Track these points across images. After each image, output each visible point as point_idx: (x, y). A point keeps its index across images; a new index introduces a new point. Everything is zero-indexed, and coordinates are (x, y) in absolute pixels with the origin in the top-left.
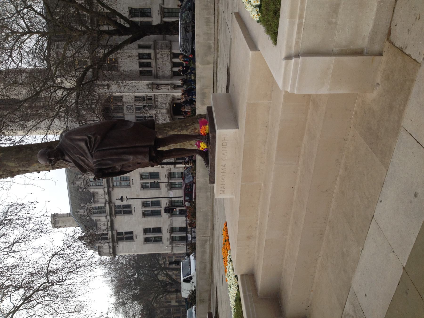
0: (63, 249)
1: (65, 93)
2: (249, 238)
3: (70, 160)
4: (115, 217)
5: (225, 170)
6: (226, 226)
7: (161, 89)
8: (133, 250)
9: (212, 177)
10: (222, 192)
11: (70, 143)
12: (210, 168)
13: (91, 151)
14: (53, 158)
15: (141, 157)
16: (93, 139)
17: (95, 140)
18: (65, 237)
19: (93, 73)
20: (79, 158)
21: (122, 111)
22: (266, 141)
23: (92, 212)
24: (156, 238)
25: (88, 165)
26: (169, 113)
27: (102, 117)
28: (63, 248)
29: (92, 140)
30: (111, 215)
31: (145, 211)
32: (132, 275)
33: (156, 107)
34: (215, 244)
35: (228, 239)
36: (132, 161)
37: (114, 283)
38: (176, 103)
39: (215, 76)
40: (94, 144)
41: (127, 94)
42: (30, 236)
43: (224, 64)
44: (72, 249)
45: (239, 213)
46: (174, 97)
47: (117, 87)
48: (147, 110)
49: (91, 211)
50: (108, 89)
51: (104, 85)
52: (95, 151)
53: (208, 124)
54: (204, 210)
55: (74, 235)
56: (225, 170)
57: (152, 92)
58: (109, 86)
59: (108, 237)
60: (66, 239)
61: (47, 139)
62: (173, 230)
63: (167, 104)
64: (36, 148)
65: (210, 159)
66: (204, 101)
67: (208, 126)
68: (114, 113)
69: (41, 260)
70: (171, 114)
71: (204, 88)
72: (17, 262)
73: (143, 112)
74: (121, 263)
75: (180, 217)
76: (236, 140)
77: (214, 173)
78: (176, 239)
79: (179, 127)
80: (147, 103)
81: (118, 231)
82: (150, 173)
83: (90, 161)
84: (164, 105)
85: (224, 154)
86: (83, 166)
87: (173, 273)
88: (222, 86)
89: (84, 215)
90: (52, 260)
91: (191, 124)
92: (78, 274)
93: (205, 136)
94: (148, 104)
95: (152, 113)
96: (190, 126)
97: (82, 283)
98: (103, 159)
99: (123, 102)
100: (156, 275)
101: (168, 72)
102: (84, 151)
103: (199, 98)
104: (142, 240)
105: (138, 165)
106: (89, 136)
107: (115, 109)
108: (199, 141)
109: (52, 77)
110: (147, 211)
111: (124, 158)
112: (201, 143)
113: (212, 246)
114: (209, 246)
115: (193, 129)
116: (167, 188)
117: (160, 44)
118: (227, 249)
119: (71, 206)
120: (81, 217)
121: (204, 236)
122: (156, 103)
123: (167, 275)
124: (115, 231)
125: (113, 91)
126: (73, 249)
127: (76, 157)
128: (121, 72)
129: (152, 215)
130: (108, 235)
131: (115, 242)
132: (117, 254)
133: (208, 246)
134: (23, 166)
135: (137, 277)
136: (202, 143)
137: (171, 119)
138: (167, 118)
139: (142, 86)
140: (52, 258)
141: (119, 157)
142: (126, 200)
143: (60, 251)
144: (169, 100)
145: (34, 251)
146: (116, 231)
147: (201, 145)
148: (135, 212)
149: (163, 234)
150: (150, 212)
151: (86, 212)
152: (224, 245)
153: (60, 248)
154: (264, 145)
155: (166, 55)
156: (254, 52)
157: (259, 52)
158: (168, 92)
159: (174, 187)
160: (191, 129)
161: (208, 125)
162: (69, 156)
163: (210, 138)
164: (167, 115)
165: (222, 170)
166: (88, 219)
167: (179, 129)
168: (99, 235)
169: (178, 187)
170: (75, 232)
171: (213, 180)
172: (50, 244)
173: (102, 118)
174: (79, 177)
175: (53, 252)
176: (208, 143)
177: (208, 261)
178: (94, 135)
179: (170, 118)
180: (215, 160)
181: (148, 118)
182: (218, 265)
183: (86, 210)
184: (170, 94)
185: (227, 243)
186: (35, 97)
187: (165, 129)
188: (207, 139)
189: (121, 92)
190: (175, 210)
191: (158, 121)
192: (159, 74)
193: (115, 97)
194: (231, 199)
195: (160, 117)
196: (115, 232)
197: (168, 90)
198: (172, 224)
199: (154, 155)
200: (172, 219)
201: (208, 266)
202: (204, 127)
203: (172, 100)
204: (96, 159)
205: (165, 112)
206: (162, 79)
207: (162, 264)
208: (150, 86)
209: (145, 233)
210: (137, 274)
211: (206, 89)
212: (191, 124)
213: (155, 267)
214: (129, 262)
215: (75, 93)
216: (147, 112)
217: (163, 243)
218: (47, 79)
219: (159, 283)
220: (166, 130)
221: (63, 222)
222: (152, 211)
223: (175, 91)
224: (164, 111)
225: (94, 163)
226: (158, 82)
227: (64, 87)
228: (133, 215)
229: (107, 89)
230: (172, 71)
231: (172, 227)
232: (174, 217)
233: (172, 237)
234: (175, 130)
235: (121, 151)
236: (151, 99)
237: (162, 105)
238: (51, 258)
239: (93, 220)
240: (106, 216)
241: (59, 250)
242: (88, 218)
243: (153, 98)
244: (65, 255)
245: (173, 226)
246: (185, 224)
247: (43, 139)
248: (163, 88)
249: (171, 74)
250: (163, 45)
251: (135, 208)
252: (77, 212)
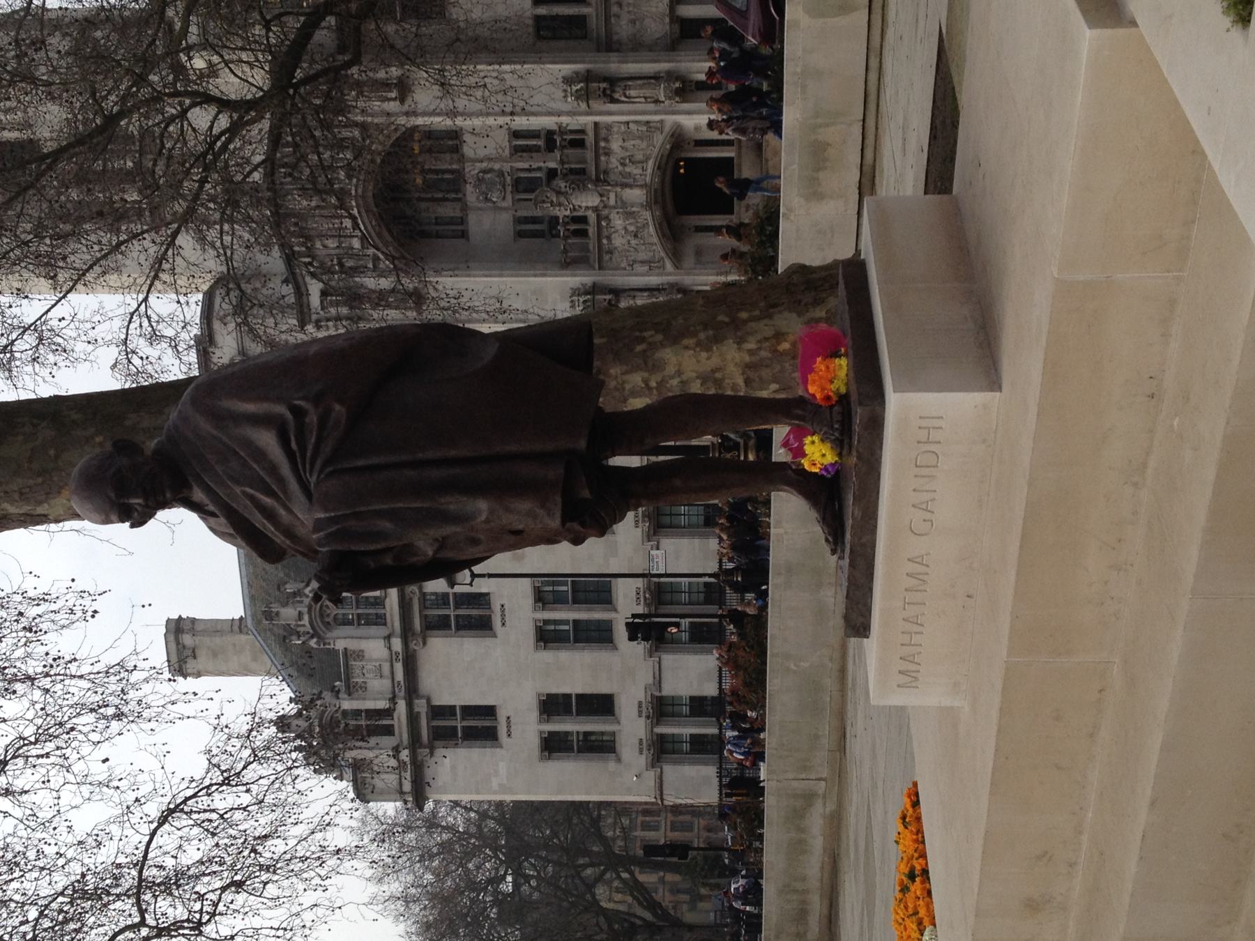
0: (208, 787)
1: (224, 122)
2: (1033, 906)
3: (211, 508)
4: (424, 644)
5: (925, 577)
6: (916, 804)
7: (623, 99)
8: (495, 783)
9: (858, 603)
10: (903, 679)
11: (215, 432)
12: (852, 565)
13: (305, 472)
14: (137, 497)
15: (525, 505)
16: (312, 418)
18: (218, 737)
19: (340, 29)
20: (252, 498)
21: (460, 195)
22: (1145, 465)
23: (330, 619)
24: (593, 738)
25: (289, 533)
26: (656, 203)
27: (376, 220)
28: (207, 782)
29: (307, 420)
30: (407, 632)
31: (546, 622)
32: (490, 881)
33: (602, 179)
34: (852, 820)
35: (925, 872)
36: (487, 521)
37: (416, 908)
38: (686, 160)
39: (874, 63)
40: (320, 440)
41: (477, 122)
42: (72, 729)
43: (921, 23)
44: (244, 788)
45: (991, 793)
46: (680, 135)
47: (440, 94)
48: (563, 190)
49: (328, 615)
50: (402, 100)
51: (386, 85)
52: (321, 472)
53: (846, 351)
54: (805, 665)
55: (251, 730)
56: (925, 577)
57: (588, 114)
58: (403, 89)
59: (393, 726)
60: (221, 744)
61: (149, 318)
62: (661, 708)
63: (651, 163)
64: (75, 416)
65: (849, 523)
66: (818, 179)
67: (843, 362)
68: (423, 205)
69: (115, 830)
70: (664, 209)
71: (819, 121)
72: (19, 834)
73: (544, 202)
74: (447, 828)
75: (696, 652)
76: (984, 441)
77: (871, 590)
78: (677, 746)
79: (706, 327)
80: (566, 160)
81: (436, 702)
83: (300, 516)
84: (636, 171)
85: (924, 506)
86: (270, 535)
87: (662, 880)
88: (905, 119)
89: (299, 629)
90: (159, 833)
91: (757, 313)
92: (265, 894)
93: (831, 407)
94: (566, 166)
95: (584, 204)
96: (753, 324)
97: (280, 933)
98: (357, 510)
99: (463, 156)
100: (590, 887)
101: (656, 26)
102: (273, 470)
103: (795, 166)
104: (534, 742)
105: (512, 539)
106: (297, 402)
107: (429, 186)
108: (798, 426)
109: (173, 52)
110: (556, 622)
111: (452, 507)
112: (808, 440)
113: (836, 823)
114: (821, 821)
115: (766, 339)
116: (639, 530)
118: (916, 913)
119: (246, 591)
120: (285, 638)
121: (803, 776)
122: (603, 158)
123: (636, 888)
124: (424, 701)
125: (420, 108)
126: (248, 791)
127: (239, 494)
128: (456, 26)
129: (577, 641)
130: (395, 715)
131: (422, 746)
132: (428, 796)
133: (816, 822)
134: (21, 494)
135: (510, 888)
136: (816, 438)
137: (667, 232)
138: (646, 225)
139: (542, 89)
140: (160, 825)
141: (426, 505)
142: (468, 580)
143: (195, 796)
144: (658, 146)
145: (87, 795)
146: (429, 700)
147: (808, 449)
148: (507, 624)
149: (619, 723)
150: (566, 628)
151: (306, 617)
152: (901, 891)
153: (194, 784)
154: (1135, 484)
156: (1108, 32)
157: (1133, 30)
158: (656, 113)
159: (670, 527)
160: (759, 337)
161: (846, 355)
162: (208, 490)
163: (856, 428)
164: (647, 215)
165: (910, 564)
166: (315, 646)
167: (702, 336)
168: (357, 713)
169: (690, 526)
170: (257, 720)
171: (861, 619)
172: (151, 764)
173: (374, 223)
175: (167, 800)
176: (841, 442)
177: (818, 884)
178: (317, 400)
179: (661, 229)
180: (876, 527)
181: (568, 223)
182: (866, 924)
183: (306, 609)
184: (662, 122)
185: (916, 887)
186: (100, 138)
187: (637, 334)
188: (842, 423)
189: (453, 113)
190: (675, 630)
191: (609, 238)
192: (617, 33)
193: (430, 134)
194: (948, 716)
195: (618, 222)
196: (421, 706)
197: (657, 101)
198: (660, 682)
199: (586, 494)
200: (659, 663)
201: (817, 906)
202: (828, 367)
203: (672, 148)
204: (326, 510)
205: (638, 201)
206: (631, 54)
207: (614, 839)
208: (579, 87)
209: (545, 717)
210: (509, 879)
211: (827, 125)
212: (757, 313)
213: (587, 853)
214: (479, 827)
215: (265, 124)
216: (562, 199)
217: (619, 760)
218: (147, 62)
219: (602, 919)
220: (643, 340)
221: (215, 655)
222: (575, 622)
223: (686, 106)
224: (636, 195)
225: (318, 526)
226: (613, 65)
227: (219, 94)
228: (495, 636)
229: (395, 99)
230: (674, 18)
231: (658, 694)
232: (667, 652)
233: (662, 737)
234: (686, 342)
235: (436, 474)
236: (579, 144)
237: (628, 169)
238: (155, 824)
239: (335, 652)
240: (388, 638)
241: (189, 793)
242: (313, 643)
243: (590, 139)
244: (214, 816)
245: (664, 693)
246: (717, 686)
247: (132, 318)
248: (633, 93)
249: (671, 29)
251: (506, 607)
252: (269, 615)
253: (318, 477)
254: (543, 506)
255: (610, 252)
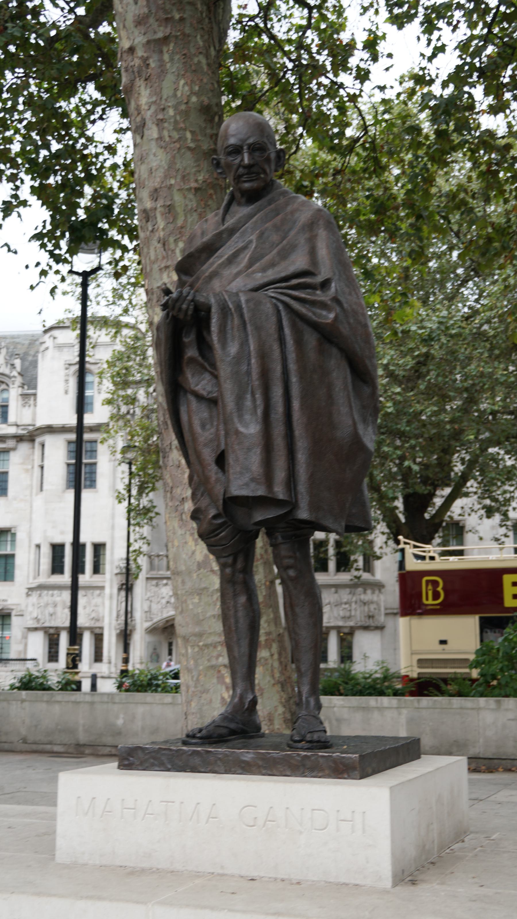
14: (249, 159)
16: (319, 296)
17: (323, 305)
82: (13, 556)
86: (211, 260)
106: (333, 285)
117: (375, 598)
155: (348, 614)
174: (18, 362)
250: (372, 607)
253: (273, 297)
254: (253, 480)
255: (157, 585)
